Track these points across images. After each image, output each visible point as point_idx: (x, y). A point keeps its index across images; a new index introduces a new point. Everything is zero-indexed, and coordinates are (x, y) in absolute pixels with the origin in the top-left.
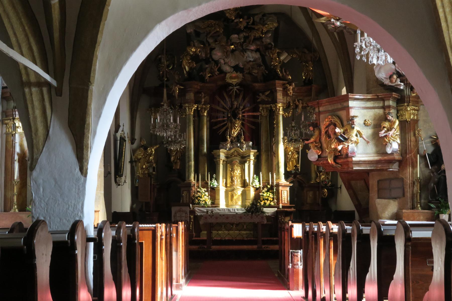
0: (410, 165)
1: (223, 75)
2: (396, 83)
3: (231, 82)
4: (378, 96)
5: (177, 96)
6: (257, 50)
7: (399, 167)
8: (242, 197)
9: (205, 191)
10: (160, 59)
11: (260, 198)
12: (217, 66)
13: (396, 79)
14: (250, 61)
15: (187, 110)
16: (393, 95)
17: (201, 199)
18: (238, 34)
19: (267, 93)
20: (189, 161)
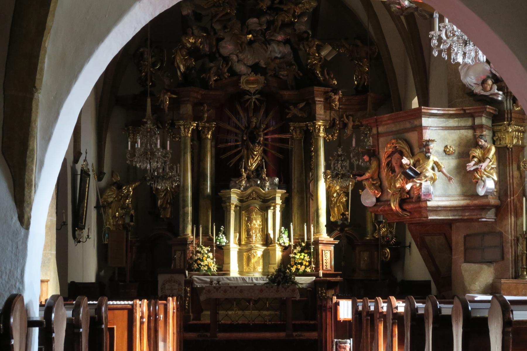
0: (513, 213)
1: (235, 78)
2: (492, 92)
3: (248, 89)
4: (465, 110)
5: (166, 109)
6: (286, 42)
7: (496, 215)
8: (263, 260)
9: (208, 250)
10: (142, 54)
12: (227, 64)
13: (492, 86)
14: (276, 58)
16: (487, 110)
17: (202, 263)
18: (258, 18)
19: (301, 105)
20: (185, 205)
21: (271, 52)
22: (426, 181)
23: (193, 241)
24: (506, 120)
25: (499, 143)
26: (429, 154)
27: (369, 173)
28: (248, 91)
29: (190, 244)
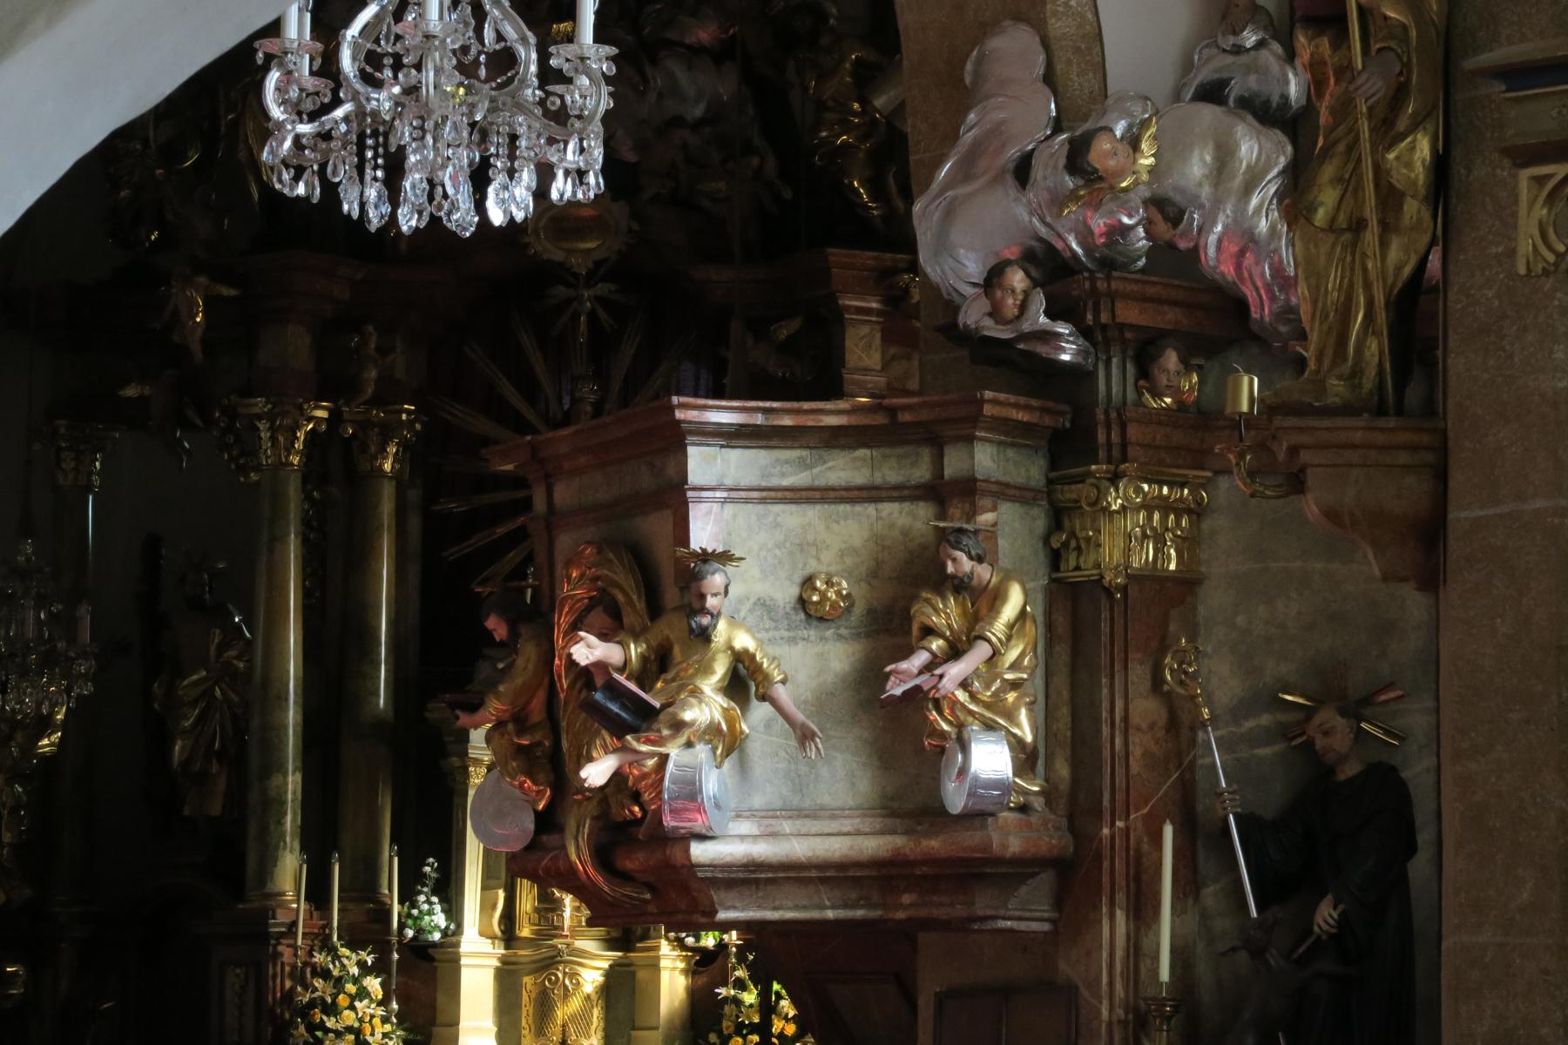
0: (1120, 897)
2: (1026, 327)
3: (559, 256)
4: (892, 412)
5: (196, 348)
6: (720, 54)
7: (1058, 904)
8: (608, 1009)
9: (361, 964)
11: (720, 1017)
13: (1026, 293)
14: (678, 121)
15: (265, 435)
16: (988, 410)
17: (330, 1023)
19: (784, 332)
20: (273, 766)
21: (660, 95)
22: (689, 745)
23: (294, 924)
24: (1102, 454)
25: (1072, 563)
26: (705, 620)
27: (498, 696)
28: (561, 265)
29: (281, 935)
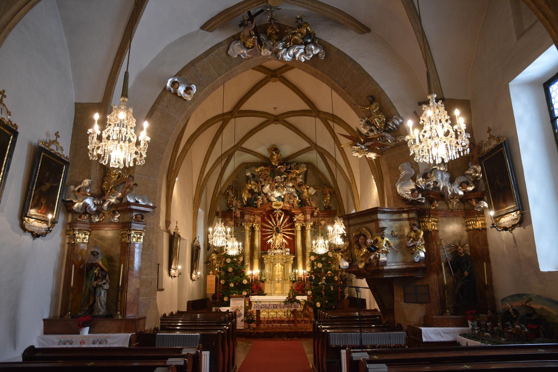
1: (270, 203)
10: (228, 193)
18: (280, 176)
